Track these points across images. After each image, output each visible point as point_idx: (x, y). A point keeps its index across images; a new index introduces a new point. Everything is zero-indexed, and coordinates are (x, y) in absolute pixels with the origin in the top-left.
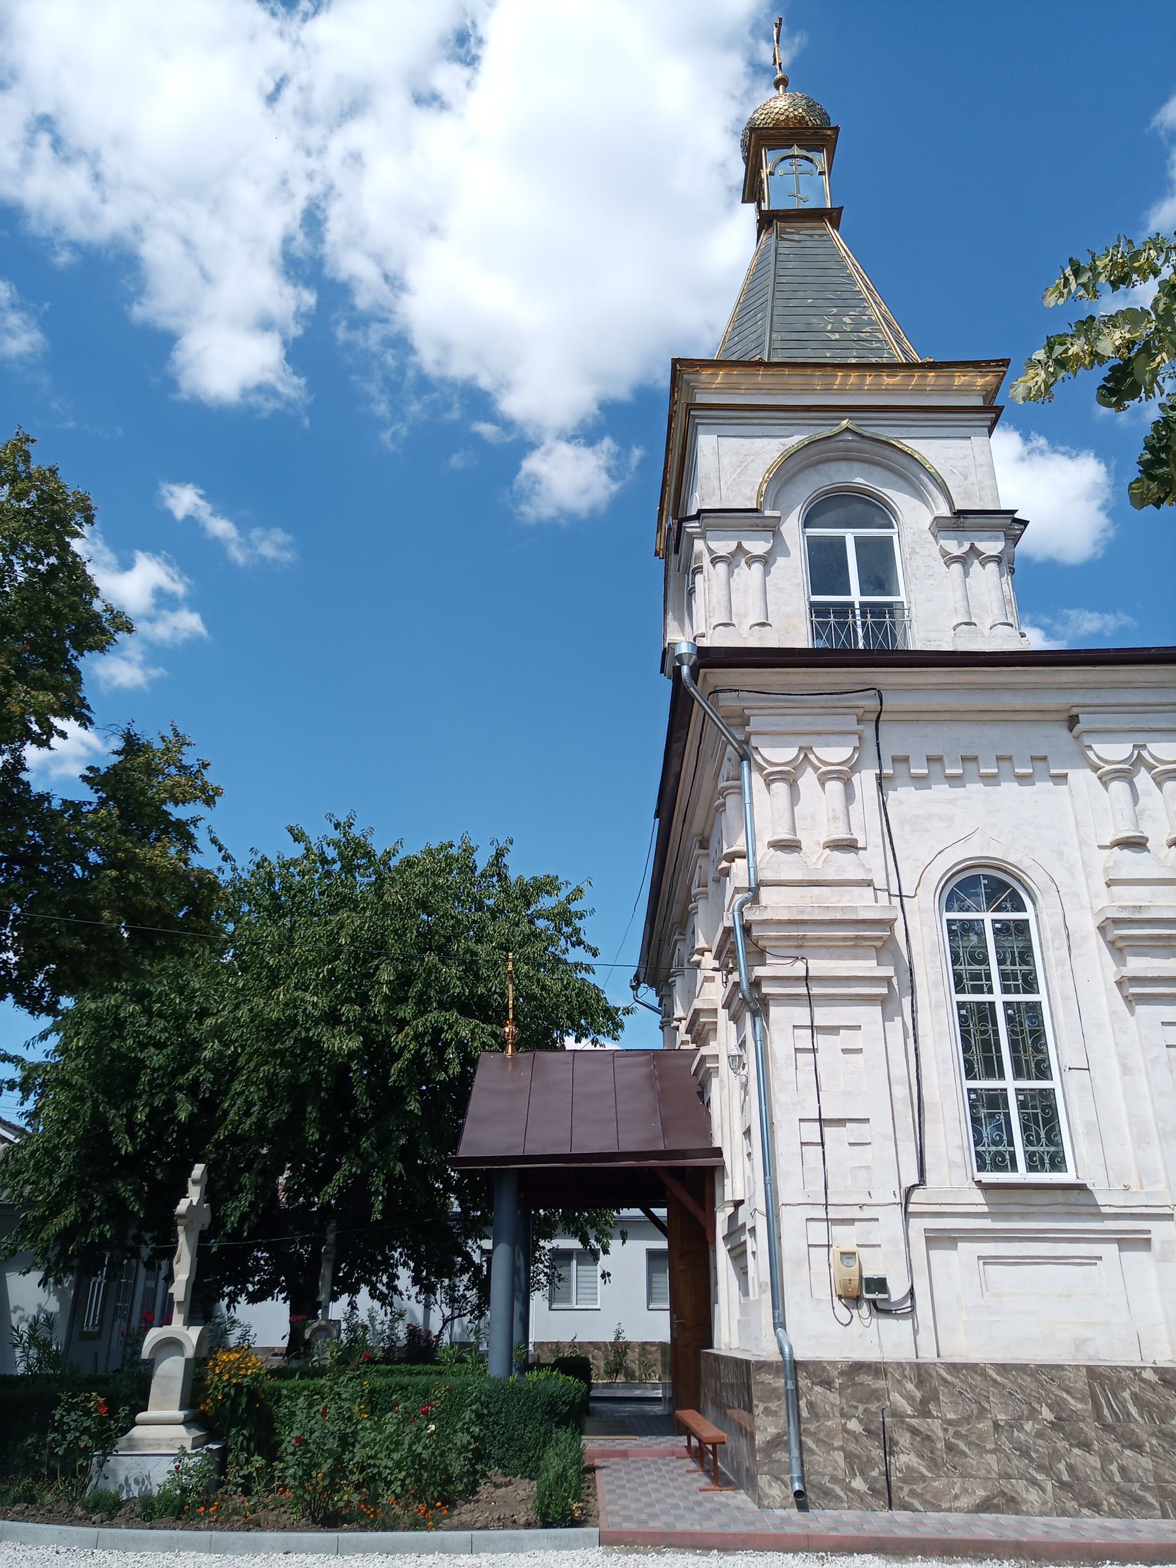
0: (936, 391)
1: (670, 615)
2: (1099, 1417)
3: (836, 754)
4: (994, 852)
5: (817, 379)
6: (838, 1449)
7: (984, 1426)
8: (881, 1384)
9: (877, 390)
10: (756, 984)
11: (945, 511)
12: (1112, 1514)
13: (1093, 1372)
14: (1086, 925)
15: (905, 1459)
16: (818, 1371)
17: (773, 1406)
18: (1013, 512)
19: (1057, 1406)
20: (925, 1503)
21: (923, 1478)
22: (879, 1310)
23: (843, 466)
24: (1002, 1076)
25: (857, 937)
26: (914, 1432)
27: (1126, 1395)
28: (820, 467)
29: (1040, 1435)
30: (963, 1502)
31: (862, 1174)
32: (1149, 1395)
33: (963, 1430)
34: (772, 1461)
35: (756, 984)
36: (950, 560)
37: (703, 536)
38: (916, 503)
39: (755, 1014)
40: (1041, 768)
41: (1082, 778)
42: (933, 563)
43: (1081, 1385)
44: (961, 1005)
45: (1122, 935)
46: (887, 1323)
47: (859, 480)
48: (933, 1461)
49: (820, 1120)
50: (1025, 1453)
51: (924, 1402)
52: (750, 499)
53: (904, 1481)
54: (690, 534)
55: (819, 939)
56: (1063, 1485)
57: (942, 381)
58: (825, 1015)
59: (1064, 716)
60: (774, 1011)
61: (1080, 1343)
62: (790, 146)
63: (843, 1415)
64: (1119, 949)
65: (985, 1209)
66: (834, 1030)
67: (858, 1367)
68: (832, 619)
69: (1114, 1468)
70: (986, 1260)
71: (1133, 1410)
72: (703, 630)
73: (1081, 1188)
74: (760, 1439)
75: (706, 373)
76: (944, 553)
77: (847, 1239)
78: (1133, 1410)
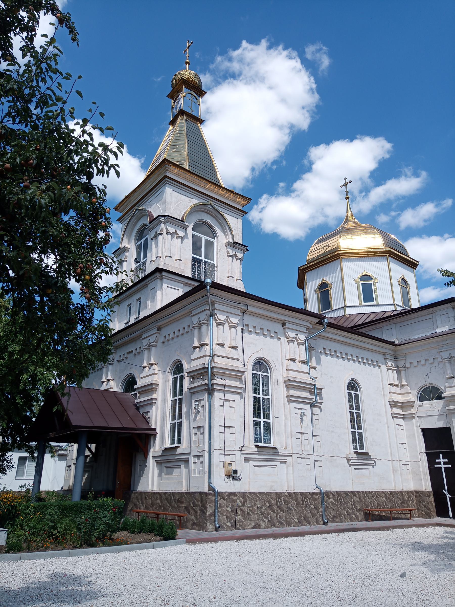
0: (231, 200)
1: (125, 236)
2: (277, 504)
3: (235, 320)
4: (268, 358)
5: (203, 183)
6: (256, 514)
7: (255, 508)
8: (235, 498)
9: (217, 193)
10: (213, 385)
11: (231, 240)
12: (277, 527)
13: (277, 494)
14: (281, 380)
15: (239, 517)
16: (221, 495)
17: (211, 505)
18: (247, 247)
19: (269, 502)
20: (242, 527)
21: (242, 521)
22: (234, 479)
23: (205, 214)
24: (260, 418)
25: (237, 375)
26: (241, 510)
27: (282, 499)
28: (200, 212)
29: (266, 509)
30: (250, 527)
31: (232, 442)
32: (286, 499)
33: (251, 509)
34: (210, 519)
35: (213, 385)
36: (229, 255)
37: (165, 223)
38: (223, 234)
39: (209, 394)
40: (275, 336)
41: (384, 367)
42: (224, 255)
43: (274, 497)
44: (350, 412)
45: (290, 384)
46: (236, 482)
47: (209, 221)
48: (244, 517)
49: (224, 426)
50: (262, 513)
51: (244, 502)
52: (179, 216)
53: (238, 522)
54: (161, 221)
55: (228, 374)
56: (269, 521)
57: (234, 198)
58: (228, 396)
59: (282, 322)
60: (216, 394)
61: (272, 487)
62: (191, 90)
63: (227, 507)
64: (288, 387)
65: (257, 453)
66: (229, 401)
67: (231, 494)
68: (197, 264)
69: (278, 516)
70: (255, 466)
71: (283, 502)
72: (160, 255)
73: (275, 448)
74: (208, 514)
75: (172, 168)
76: (228, 253)
77: (228, 459)
78: (283, 502)
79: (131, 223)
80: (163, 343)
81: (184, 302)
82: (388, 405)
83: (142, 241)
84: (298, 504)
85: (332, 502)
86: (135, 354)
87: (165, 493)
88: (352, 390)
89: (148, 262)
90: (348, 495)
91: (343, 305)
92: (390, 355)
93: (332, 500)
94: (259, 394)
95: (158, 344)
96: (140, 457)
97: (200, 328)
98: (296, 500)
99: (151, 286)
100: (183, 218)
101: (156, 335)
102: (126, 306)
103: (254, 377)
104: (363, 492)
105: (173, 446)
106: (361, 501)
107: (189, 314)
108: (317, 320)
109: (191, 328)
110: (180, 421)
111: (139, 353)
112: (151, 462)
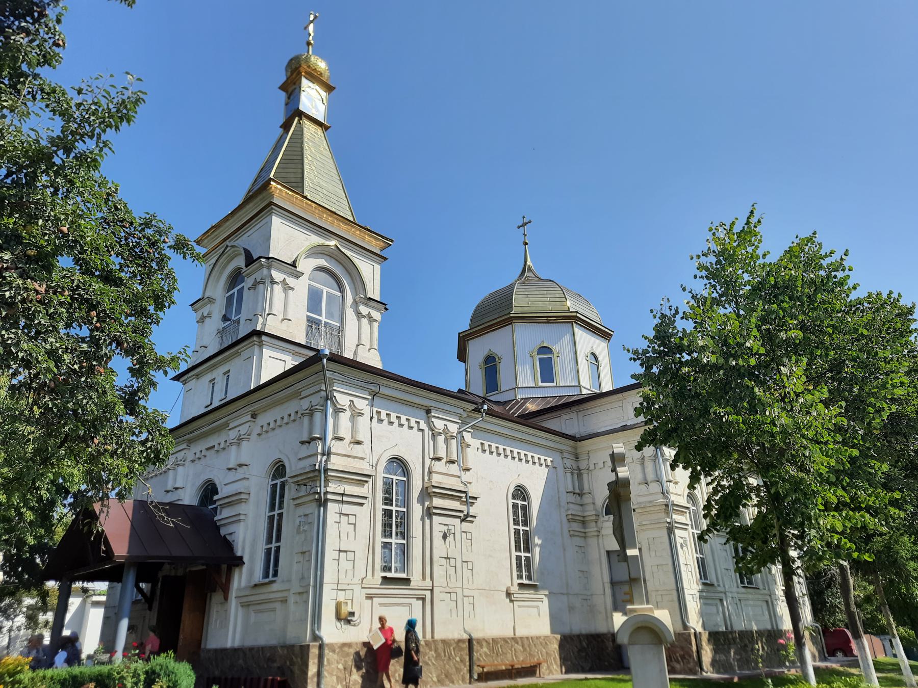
10: (326, 493)
58: (346, 509)
60: (330, 505)
70: (381, 605)
79: (219, 263)
80: (259, 435)
81: (291, 379)
82: (565, 519)
83: (235, 290)
84: (438, 656)
85: (485, 653)
86: (218, 451)
87: (251, 649)
88: (518, 499)
89: (242, 322)
90: (507, 642)
91: (514, 386)
92: (569, 452)
93: (485, 649)
94: (391, 505)
95: (251, 437)
96: (217, 597)
97: (311, 415)
98: (436, 651)
99: (245, 354)
100: (295, 262)
101: (248, 424)
102: (221, 374)
103: (385, 483)
104: (527, 638)
105: (267, 580)
106: (525, 650)
107: (297, 395)
108: (473, 407)
109: (299, 415)
110: (277, 544)
111: (224, 449)
112: (233, 602)
